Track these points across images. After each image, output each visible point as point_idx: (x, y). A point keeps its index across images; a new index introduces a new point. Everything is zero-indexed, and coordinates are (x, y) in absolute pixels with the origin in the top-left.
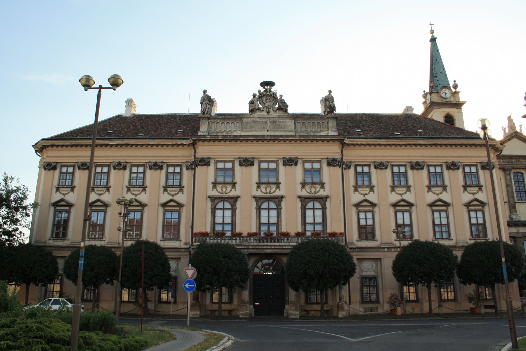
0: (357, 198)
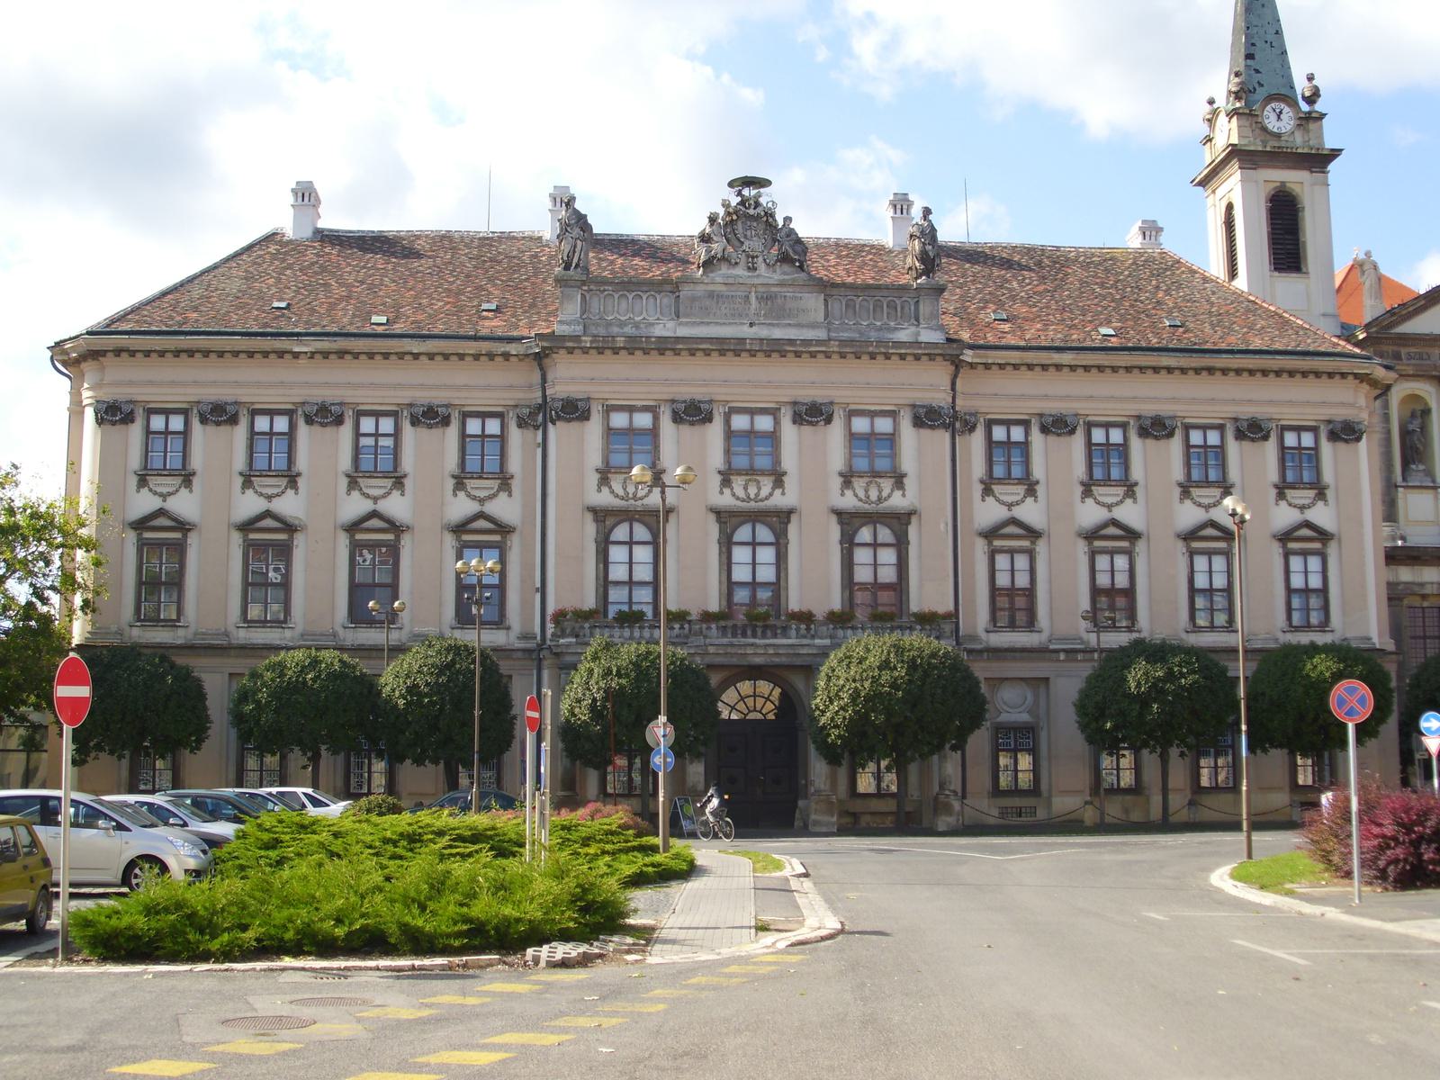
0: (988, 512)
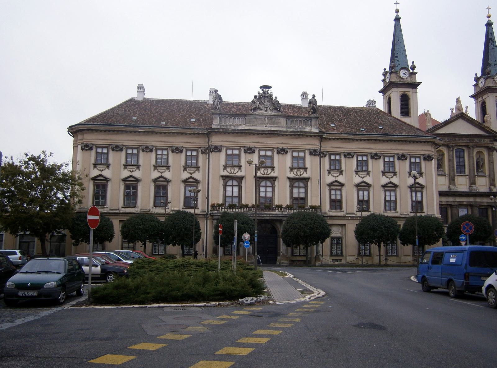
0: (329, 179)
